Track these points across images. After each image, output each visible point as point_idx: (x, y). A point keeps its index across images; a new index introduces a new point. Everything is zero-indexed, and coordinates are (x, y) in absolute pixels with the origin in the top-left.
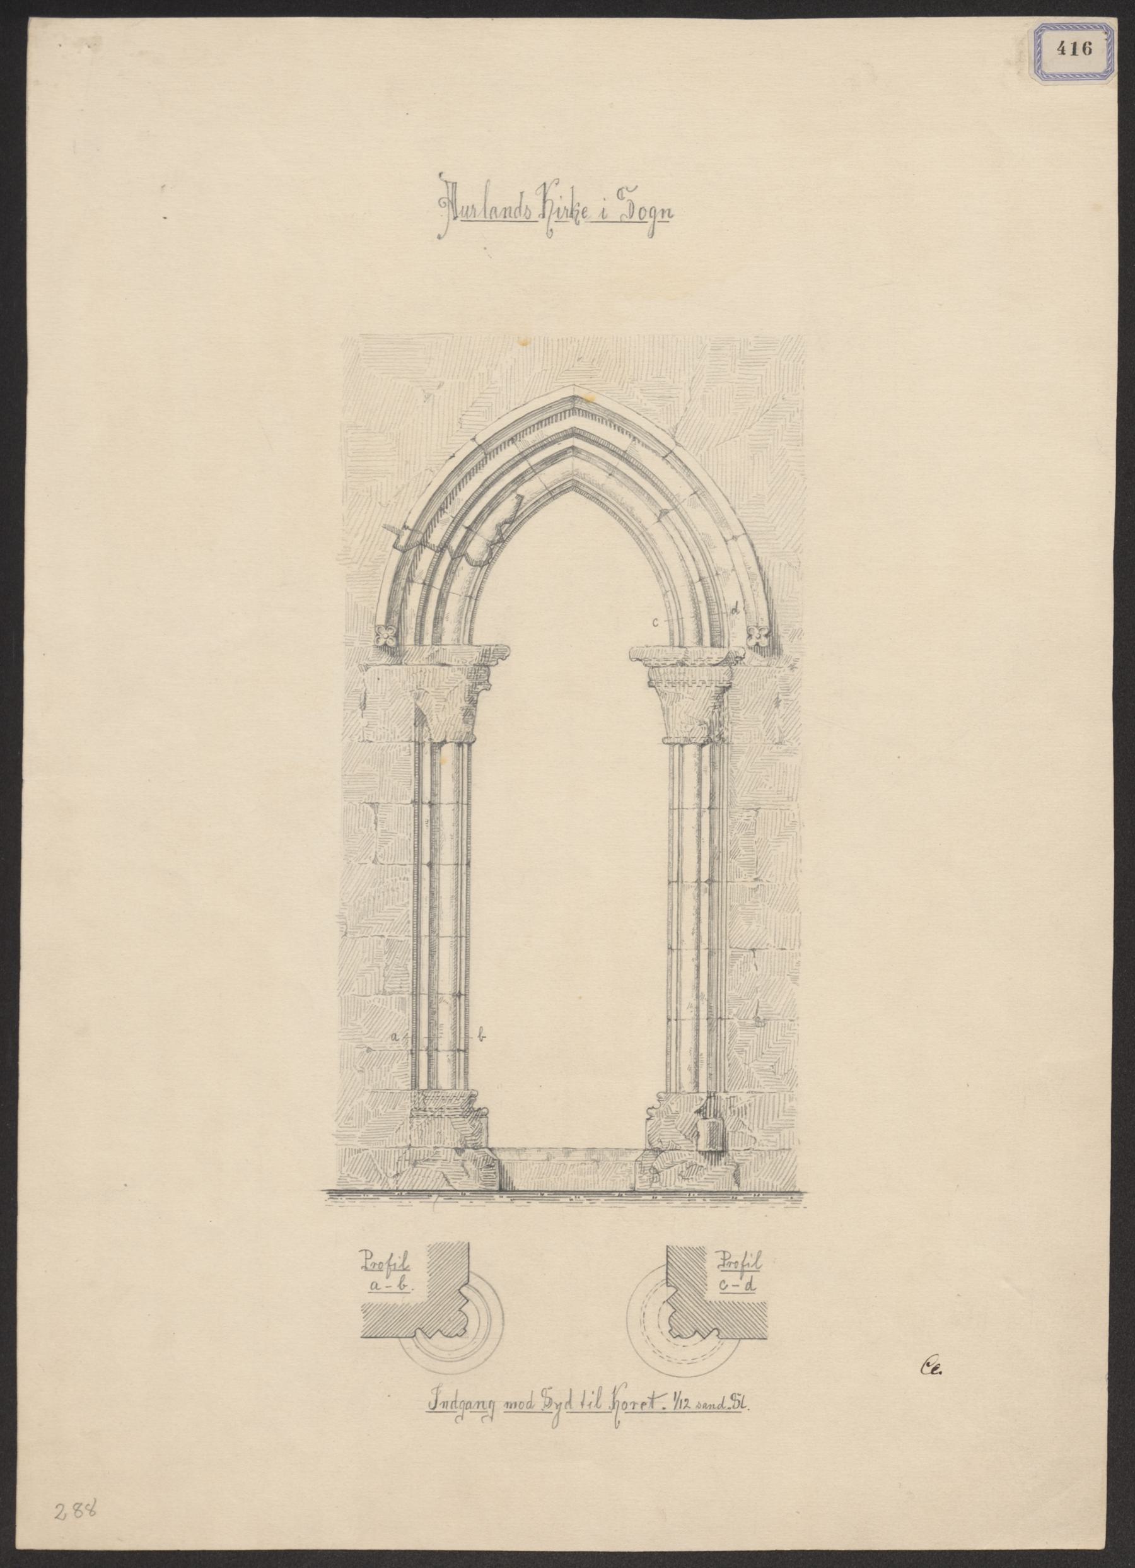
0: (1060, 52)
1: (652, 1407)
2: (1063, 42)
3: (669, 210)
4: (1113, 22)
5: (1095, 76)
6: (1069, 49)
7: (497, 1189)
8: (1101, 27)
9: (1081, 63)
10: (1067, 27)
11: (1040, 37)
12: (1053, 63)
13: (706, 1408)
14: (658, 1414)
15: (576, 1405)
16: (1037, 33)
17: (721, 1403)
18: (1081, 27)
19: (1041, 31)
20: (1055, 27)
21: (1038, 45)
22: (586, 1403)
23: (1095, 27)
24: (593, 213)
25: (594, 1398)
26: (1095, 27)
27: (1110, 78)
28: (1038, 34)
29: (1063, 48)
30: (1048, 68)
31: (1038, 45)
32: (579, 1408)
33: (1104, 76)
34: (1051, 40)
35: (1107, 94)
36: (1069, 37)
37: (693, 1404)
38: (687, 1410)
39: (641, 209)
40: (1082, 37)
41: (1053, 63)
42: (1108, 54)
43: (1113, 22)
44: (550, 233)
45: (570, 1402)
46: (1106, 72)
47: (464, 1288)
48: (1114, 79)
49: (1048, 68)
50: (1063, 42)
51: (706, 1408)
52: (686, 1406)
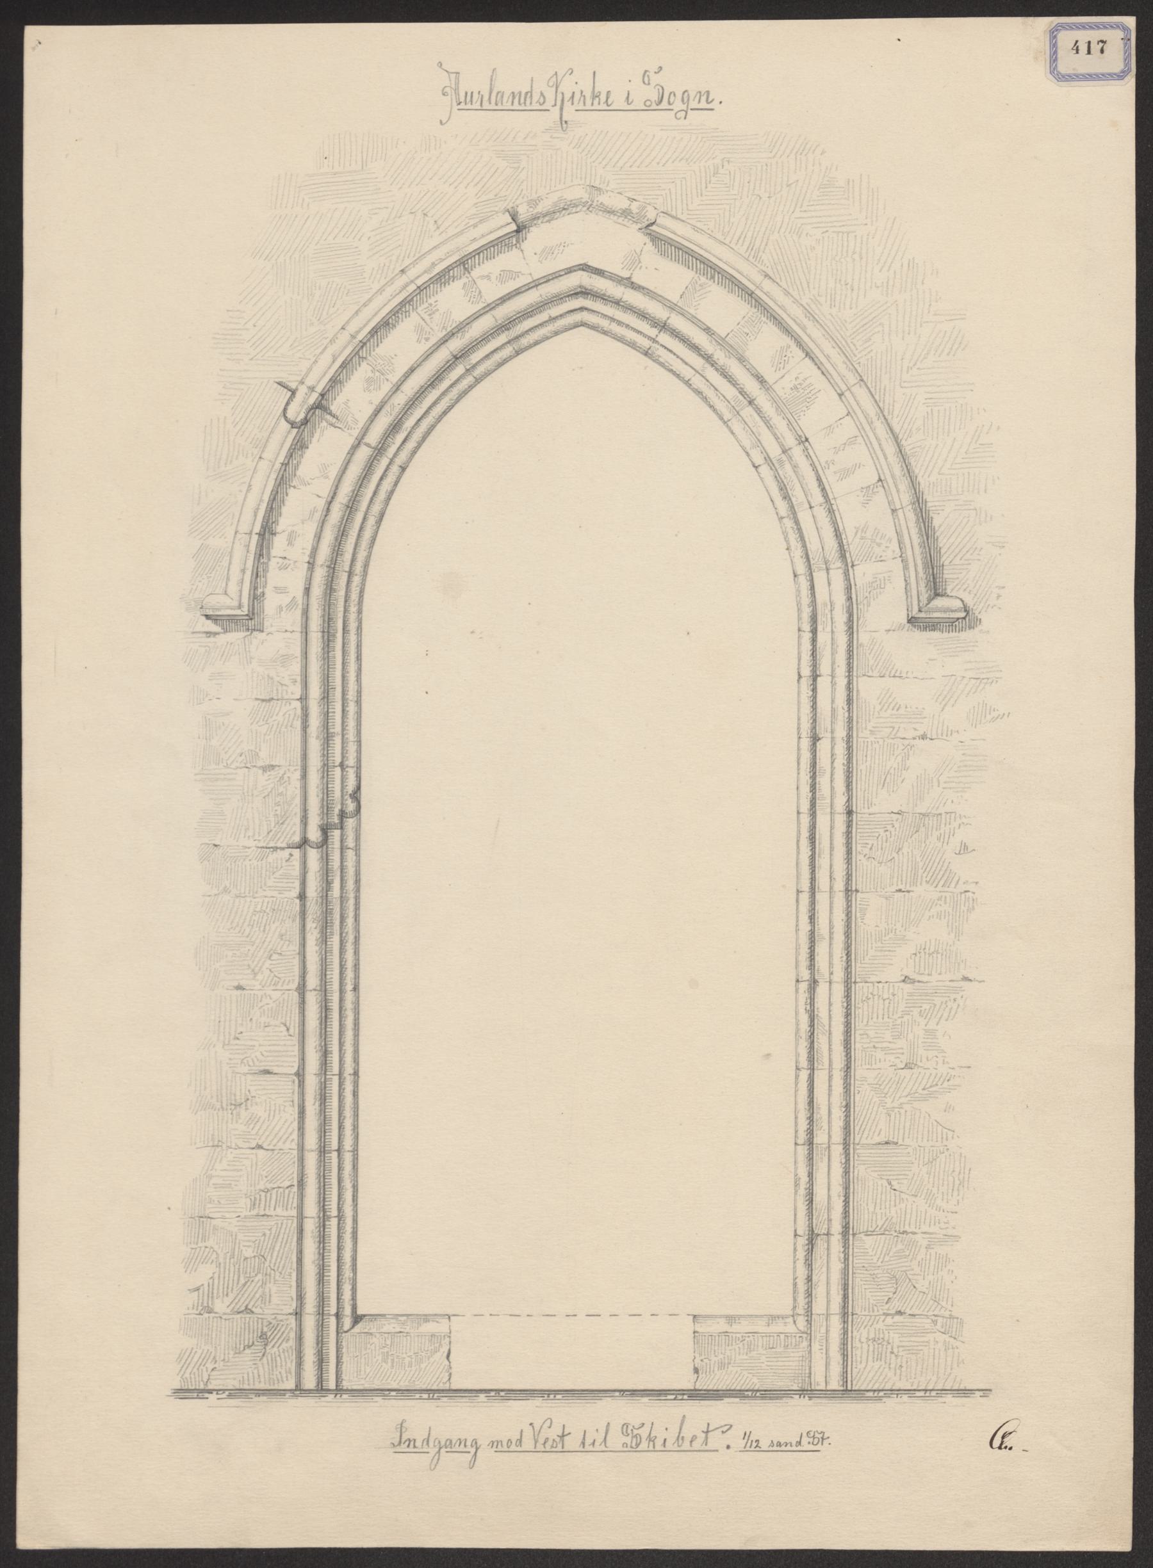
0: (1075, 52)
1: (664, 1446)
2: (1077, 42)
3: (708, 92)
4: (1130, 21)
5: (1112, 76)
6: (1083, 48)
7: (293, 1386)
8: (1117, 26)
9: (1093, 63)
10: (1083, 27)
11: (1055, 37)
12: (1068, 62)
13: (779, 1446)
14: (661, 1453)
15: (528, 1444)
16: (1053, 32)
17: (799, 1440)
18: (1097, 27)
19: (1057, 30)
20: (1071, 27)
21: (1054, 46)
22: (588, 1441)
23: (1111, 26)
24: (618, 101)
25: (600, 1438)
26: (1112, 27)
27: (1126, 79)
28: (1053, 34)
29: (1078, 47)
30: (1063, 68)
31: (1054, 46)
32: (591, 1448)
33: (1121, 76)
34: (1066, 39)
35: (1125, 93)
36: (1083, 36)
37: (764, 1444)
38: (758, 1449)
39: (671, 93)
40: (1094, 35)
41: (1068, 62)
42: (1125, 53)
43: (1130, 21)
44: (564, 125)
45: (520, 1440)
46: (1123, 72)
47: (330, 1388)
48: (1130, 83)
49: (1063, 68)
50: (1077, 42)
51: (779, 1446)
52: (757, 1446)
